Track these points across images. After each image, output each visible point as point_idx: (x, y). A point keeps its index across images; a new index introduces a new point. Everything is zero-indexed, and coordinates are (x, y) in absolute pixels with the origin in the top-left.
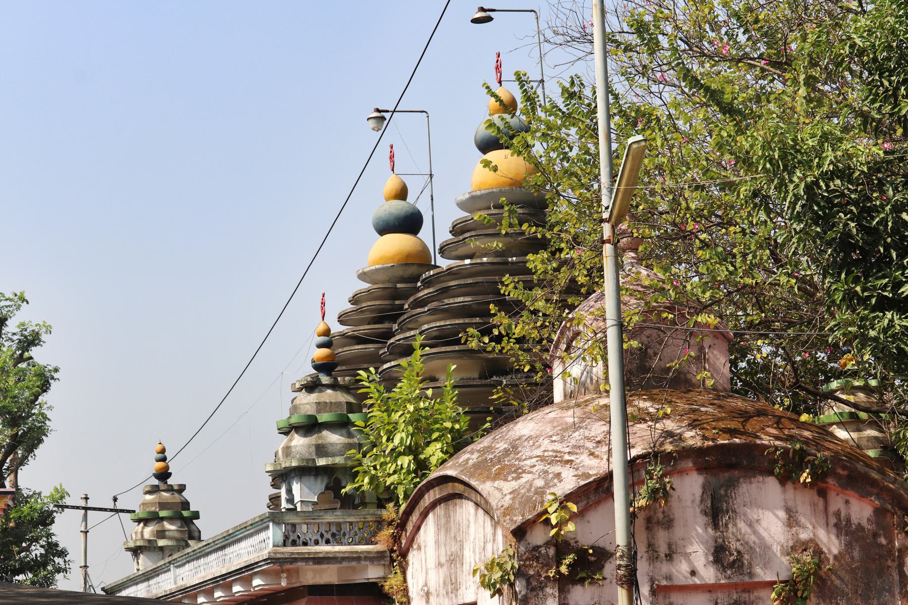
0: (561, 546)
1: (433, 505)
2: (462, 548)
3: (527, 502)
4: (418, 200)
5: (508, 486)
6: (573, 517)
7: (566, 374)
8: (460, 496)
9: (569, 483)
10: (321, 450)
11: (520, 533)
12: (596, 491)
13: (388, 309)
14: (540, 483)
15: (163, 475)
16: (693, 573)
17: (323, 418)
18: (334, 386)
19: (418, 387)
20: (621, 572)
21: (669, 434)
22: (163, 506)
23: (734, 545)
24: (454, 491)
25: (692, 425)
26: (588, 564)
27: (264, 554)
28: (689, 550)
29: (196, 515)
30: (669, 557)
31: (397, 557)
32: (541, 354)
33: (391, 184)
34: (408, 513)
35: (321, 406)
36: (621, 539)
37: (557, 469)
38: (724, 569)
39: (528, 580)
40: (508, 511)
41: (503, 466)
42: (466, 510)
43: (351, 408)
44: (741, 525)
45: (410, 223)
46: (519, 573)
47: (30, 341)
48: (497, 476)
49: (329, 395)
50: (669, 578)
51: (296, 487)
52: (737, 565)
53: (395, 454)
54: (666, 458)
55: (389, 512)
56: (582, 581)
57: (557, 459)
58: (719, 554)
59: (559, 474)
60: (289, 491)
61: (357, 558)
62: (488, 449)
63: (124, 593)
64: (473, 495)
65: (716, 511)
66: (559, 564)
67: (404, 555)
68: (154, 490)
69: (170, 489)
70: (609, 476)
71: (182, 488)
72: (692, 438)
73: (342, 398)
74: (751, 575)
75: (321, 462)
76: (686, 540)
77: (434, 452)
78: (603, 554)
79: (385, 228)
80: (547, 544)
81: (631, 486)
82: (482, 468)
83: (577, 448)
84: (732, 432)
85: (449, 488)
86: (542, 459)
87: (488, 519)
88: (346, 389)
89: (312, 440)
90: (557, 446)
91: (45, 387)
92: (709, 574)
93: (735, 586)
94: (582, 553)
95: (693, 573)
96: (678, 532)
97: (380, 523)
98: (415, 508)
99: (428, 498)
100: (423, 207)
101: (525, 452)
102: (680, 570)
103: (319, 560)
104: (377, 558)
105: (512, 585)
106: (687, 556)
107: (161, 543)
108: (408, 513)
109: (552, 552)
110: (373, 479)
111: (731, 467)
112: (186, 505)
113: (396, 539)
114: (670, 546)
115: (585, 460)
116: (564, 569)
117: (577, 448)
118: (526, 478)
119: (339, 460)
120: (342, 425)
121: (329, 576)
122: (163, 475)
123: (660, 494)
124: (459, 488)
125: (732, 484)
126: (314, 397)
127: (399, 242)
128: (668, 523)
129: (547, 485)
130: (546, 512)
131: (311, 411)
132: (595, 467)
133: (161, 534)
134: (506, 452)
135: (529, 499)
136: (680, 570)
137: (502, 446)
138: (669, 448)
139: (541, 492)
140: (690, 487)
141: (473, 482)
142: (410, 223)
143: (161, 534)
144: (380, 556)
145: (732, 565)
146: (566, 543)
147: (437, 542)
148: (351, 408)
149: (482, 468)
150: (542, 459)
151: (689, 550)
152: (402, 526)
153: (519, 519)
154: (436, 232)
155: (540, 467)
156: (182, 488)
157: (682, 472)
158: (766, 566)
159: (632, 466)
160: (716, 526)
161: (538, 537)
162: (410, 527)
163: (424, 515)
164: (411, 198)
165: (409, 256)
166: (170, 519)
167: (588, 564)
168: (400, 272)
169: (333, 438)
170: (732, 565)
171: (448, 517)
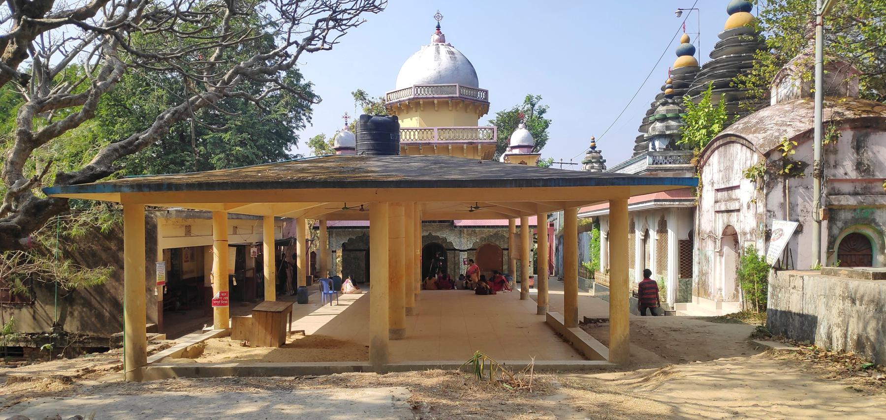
0: (786, 161)
1: (718, 147)
2: (733, 163)
3: (771, 142)
4: (693, 42)
5: (761, 136)
6: (794, 147)
7: (777, 93)
8: (733, 142)
9: (791, 133)
10: (668, 128)
11: (767, 155)
12: (806, 136)
13: (683, 84)
14: (777, 134)
15: (593, 147)
16: (846, 174)
17: (669, 115)
18: (673, 103)
19: (706, 104)
20: (816, 172)
21: (837, 113)
22: (593, 158)
23: (866, 162)
24: (730, 140)
25: (848, 109)
26: (797, 169)
27: (645, 168)
28: (844, 163)
29: (605, 161)
30: (835, 167)
31: (698, 169)
32: (764, 85)
33: (683, 37)
34: (705, 151)
35: (668, 111)
36: (817, 157)
37: (785, 128)
38: (861, 172)
39: (770, 175)
40: (762, 146)
41: (758, 128)
42: (736, 148)
43: (680, 111)
44: (870, 153)
45: (690, 51)
46: (766, 172)
47: (543, 111)
48: (754, 132)
49: (671, 107)
50: (834, 175)
51: (657, 143)
52: (867, 171)
53: (698, 130)
54: (838, 123)
55: (696, 152)
56: (794, 176)
57: (783, 124)
58: (859, 166)
59: (785, 131)
60: (653, 145)
61: (682, 169)
62: (748, 122)
63: (618, 172)
64: (741, 141)
65: (859, 146)
66: (784, 168)
67: (702, 167)
68: (590, 152)
69: (596, 152)
70: (811, 131)
71: (600, 152)
72: (849, 114)
73: (677, 108)
74: (873, 175)
75: (668, 132)
76: (843, 159)
77: (716, 127)
78: (805, 165)
79: (680, 54)
80: (780, 160)
81: (823, 134)
82: (746, 129)
83: (793, 120)
84: (868, 112)
85: (728, 139)
86: (776, 124)
87: (748, 150)
88: (678, 104)
89: (665, 124)
90: (784, 119)
91: (547, 126)
92: (853, 175)
93: (865, 180)
94: (795, 164)
95: (846, 174)
96: (840, 155)
97: (692, 156)
98: (709, 147)
99: (716, 145)
100: (696, 46)
101: (767, 122)
102: (840, 172)
103: (666, 170)
104: (689, 169)
105: (762, 177)
106: (843, 166)
107: (592, 171)
108: (705, 151)
109: (781, 163)
110: (689, 139)
111: (868, 127)
112: (601, 157)
113: (699, 162)
114: (835, 162)
115: (799, 124)
116: (787, 171)
117: (793, 120)
118: (769, 132)
119: (675, 131)
120: (676, 118)
121: (670, 175)
122: (593, 147)
123: (835, 138)
124: (734, 139)
125: (867, 135)
126: (665, 108)
127: (686, 59)
128: (835, 152)
129: (780, 134)
130: (782, 145)
131: (664, 113)
132: (804, 127)
133: (592, 167)
134: (757, 123)
135: (772, 141)
136: (840, 172)
137: (754, 121)
138: (838, 119)
139: (778, 138)
140: (847, 136)
141: (742, 135)
142: (690, 51)
143: (592, 167)
144: (691, 168)
145: (864, 171)
146: (788, 160)
147: (719, 162)
148: (680, 111)
149: (746, 129)
150: (776, 124)
151: (844, 163)
152: (702, 156)
153: (768, 149)
154: (703, 58)
155: (776, 127)
156: (600, 152)
157: (843, 129)
158: (881, 171)
159: (824, 125)
160: (858, 154)
161: (776, 156)
162: (705, 157)
163: (713, 152)
164: (691, 42)
165: (690, 63)
166: (596, 162)
167: (797, 169)
168: (687, 70)
169: (673, 123)
170: (864, 171)
171: (726, 152)
